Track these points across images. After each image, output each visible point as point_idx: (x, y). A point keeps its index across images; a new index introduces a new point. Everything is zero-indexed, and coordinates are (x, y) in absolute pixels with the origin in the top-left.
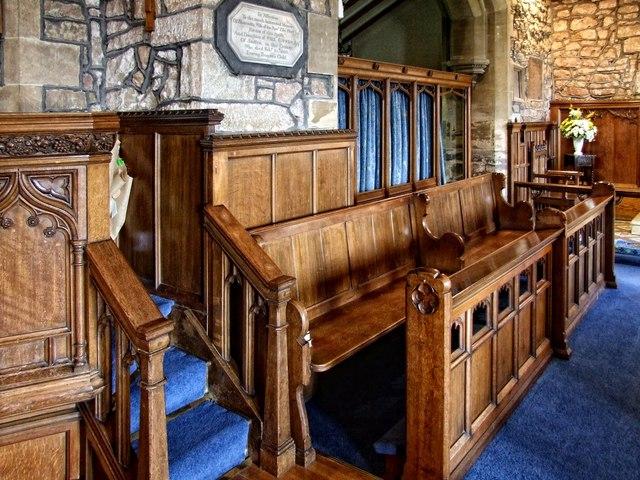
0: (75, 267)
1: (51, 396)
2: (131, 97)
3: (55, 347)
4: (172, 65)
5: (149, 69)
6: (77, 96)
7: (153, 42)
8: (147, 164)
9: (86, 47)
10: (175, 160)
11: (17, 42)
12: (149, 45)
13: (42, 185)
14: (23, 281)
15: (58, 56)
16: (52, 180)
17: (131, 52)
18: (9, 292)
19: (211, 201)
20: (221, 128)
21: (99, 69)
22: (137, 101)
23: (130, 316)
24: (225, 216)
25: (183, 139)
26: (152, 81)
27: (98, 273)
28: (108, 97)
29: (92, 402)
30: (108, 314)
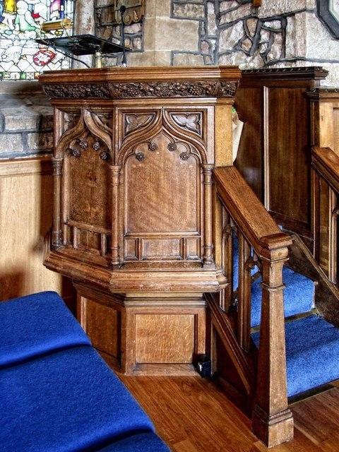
0: (204, 185)
1: (186, 283)
2: (241, 59)
3: (188, 246)
4: (277, 33)
5: (257, 36)
6: (197, 58)
7: (260, 15)
8: (257, 116)
9: (204, 22)
10: (282, 109)
11: (154, 20)
12: (256, 18)
13: (181, 120)
14: (164, 191)
15: (182, 29)
16: (187, 116)
17: (240, 24)
18: (154, 199)
19: (317, 143)
20: (325, 83)
21: (214, 38)
22: (246, 62)
23: (254, 228)
24: (331, 157)
25: (289, 92)
26: (259, 46)
27: (223, 189)
28: (221, 59)
29: (217, 295)
30: (232, 225)
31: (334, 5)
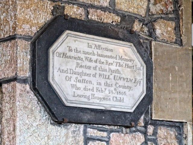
31: (55, 71)
